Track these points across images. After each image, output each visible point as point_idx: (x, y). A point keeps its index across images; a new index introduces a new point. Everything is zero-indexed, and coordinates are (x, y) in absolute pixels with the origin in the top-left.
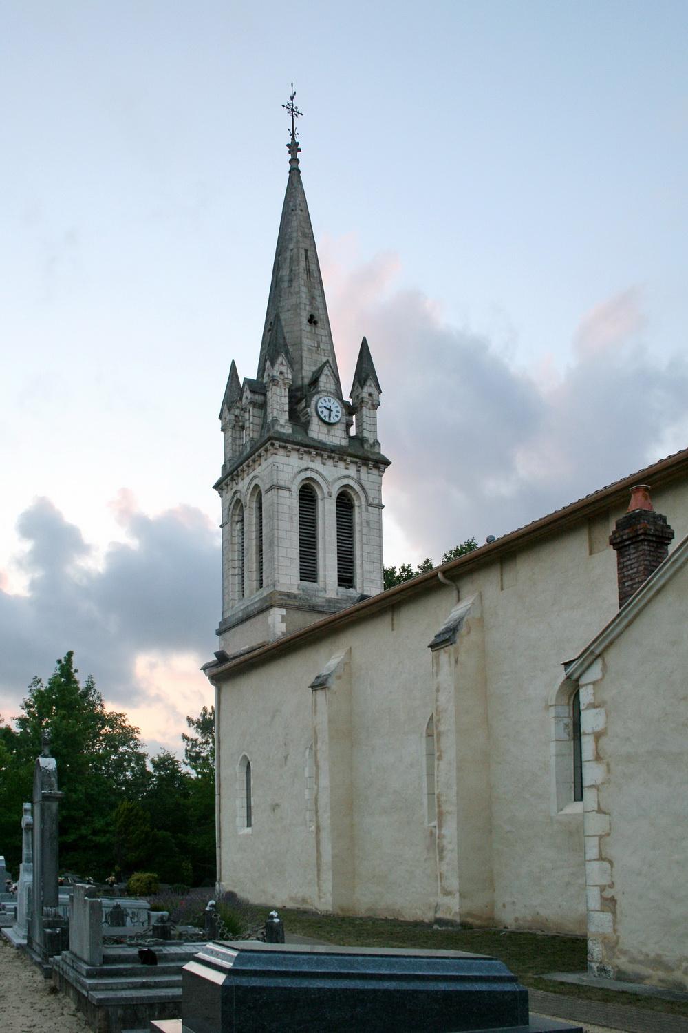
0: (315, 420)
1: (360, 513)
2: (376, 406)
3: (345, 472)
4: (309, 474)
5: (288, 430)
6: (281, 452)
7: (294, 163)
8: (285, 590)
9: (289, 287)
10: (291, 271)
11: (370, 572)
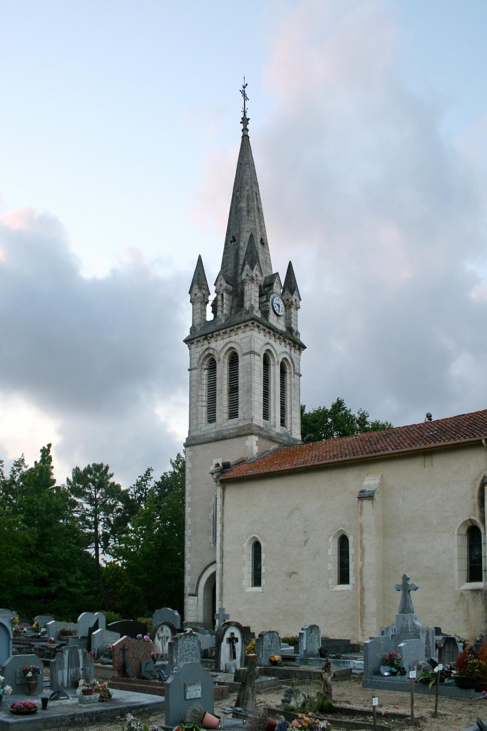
0: (271, 311)
1: (290, 377)
2: (298, 308)
4: (269, 347)
5: (259, 315)
6: (256, 329)
7: (246, 132)
8: (257, 424)
9: (247, 216)
10: (248, 205)
11: (295, 418)
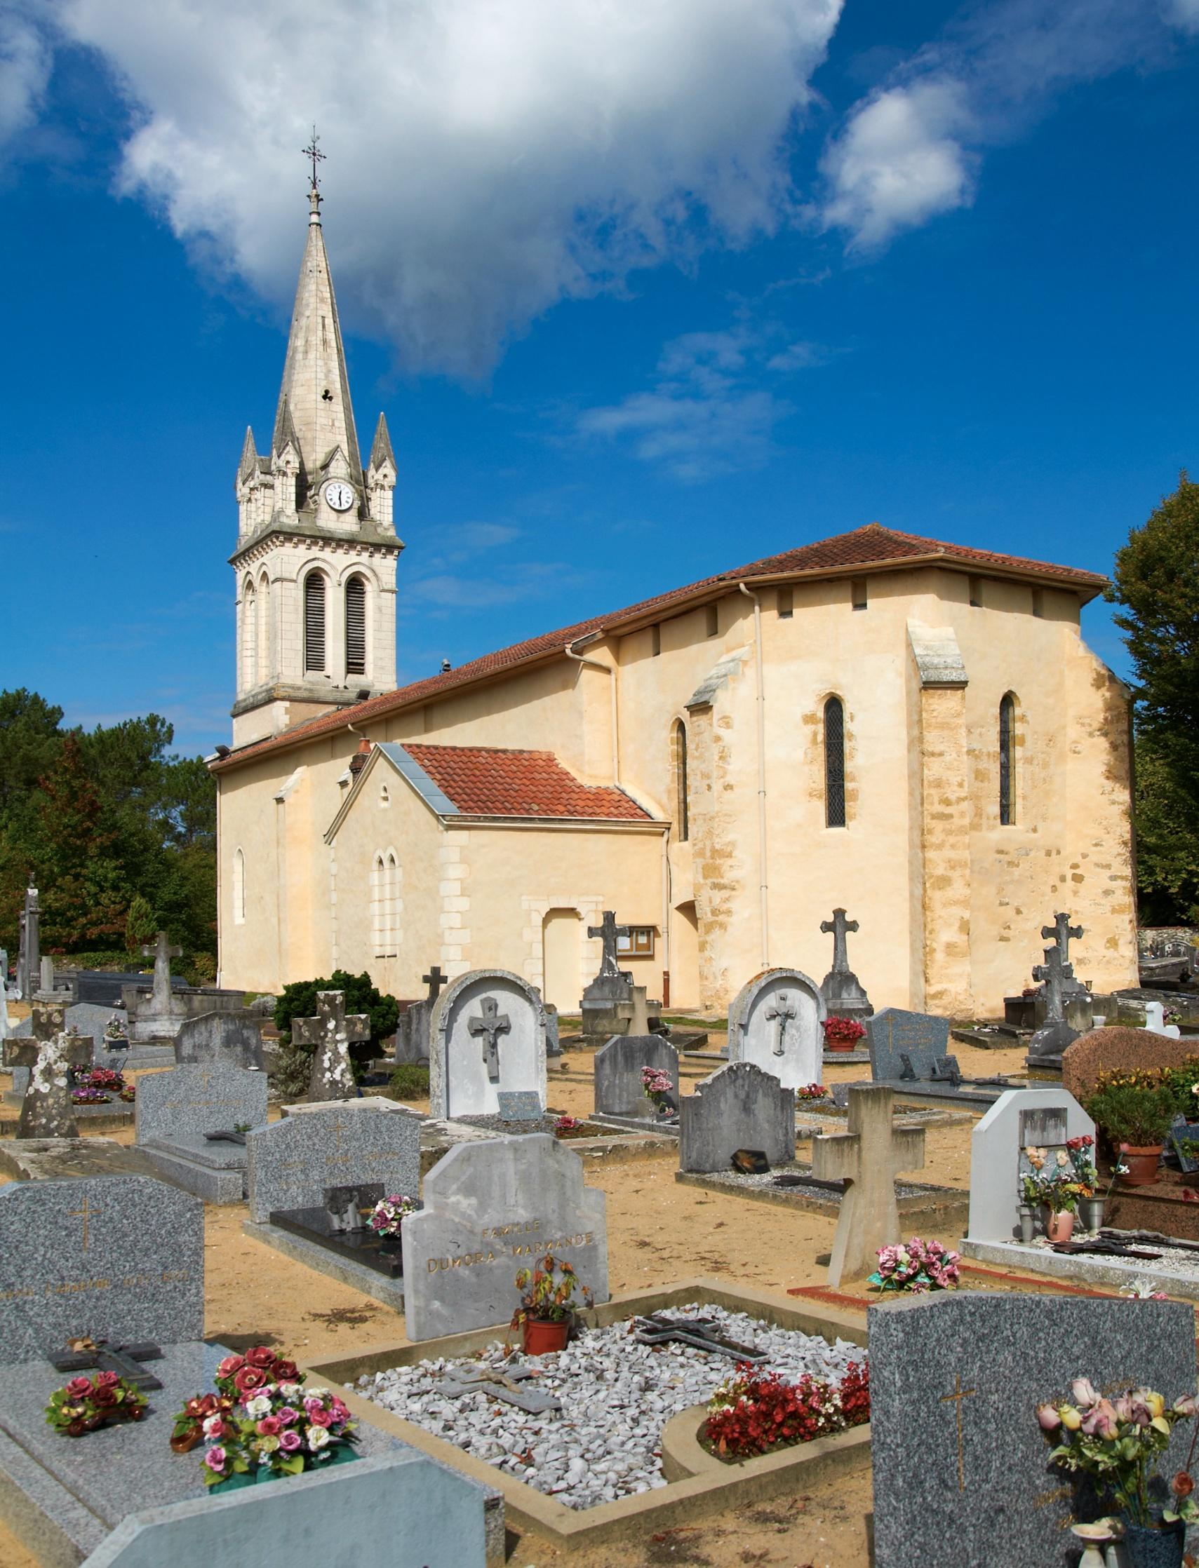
0: (324, 507)
3: (357, 559)
